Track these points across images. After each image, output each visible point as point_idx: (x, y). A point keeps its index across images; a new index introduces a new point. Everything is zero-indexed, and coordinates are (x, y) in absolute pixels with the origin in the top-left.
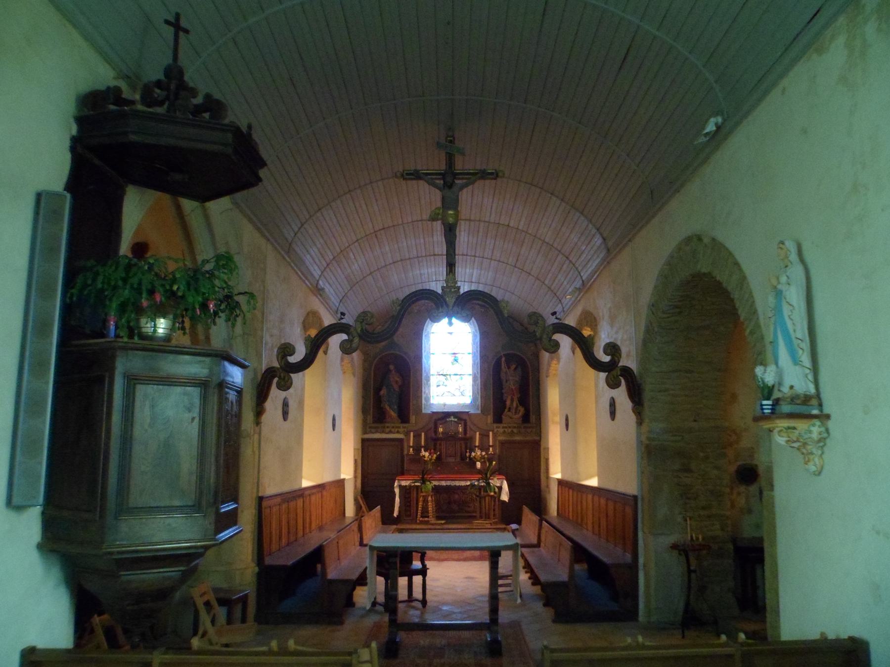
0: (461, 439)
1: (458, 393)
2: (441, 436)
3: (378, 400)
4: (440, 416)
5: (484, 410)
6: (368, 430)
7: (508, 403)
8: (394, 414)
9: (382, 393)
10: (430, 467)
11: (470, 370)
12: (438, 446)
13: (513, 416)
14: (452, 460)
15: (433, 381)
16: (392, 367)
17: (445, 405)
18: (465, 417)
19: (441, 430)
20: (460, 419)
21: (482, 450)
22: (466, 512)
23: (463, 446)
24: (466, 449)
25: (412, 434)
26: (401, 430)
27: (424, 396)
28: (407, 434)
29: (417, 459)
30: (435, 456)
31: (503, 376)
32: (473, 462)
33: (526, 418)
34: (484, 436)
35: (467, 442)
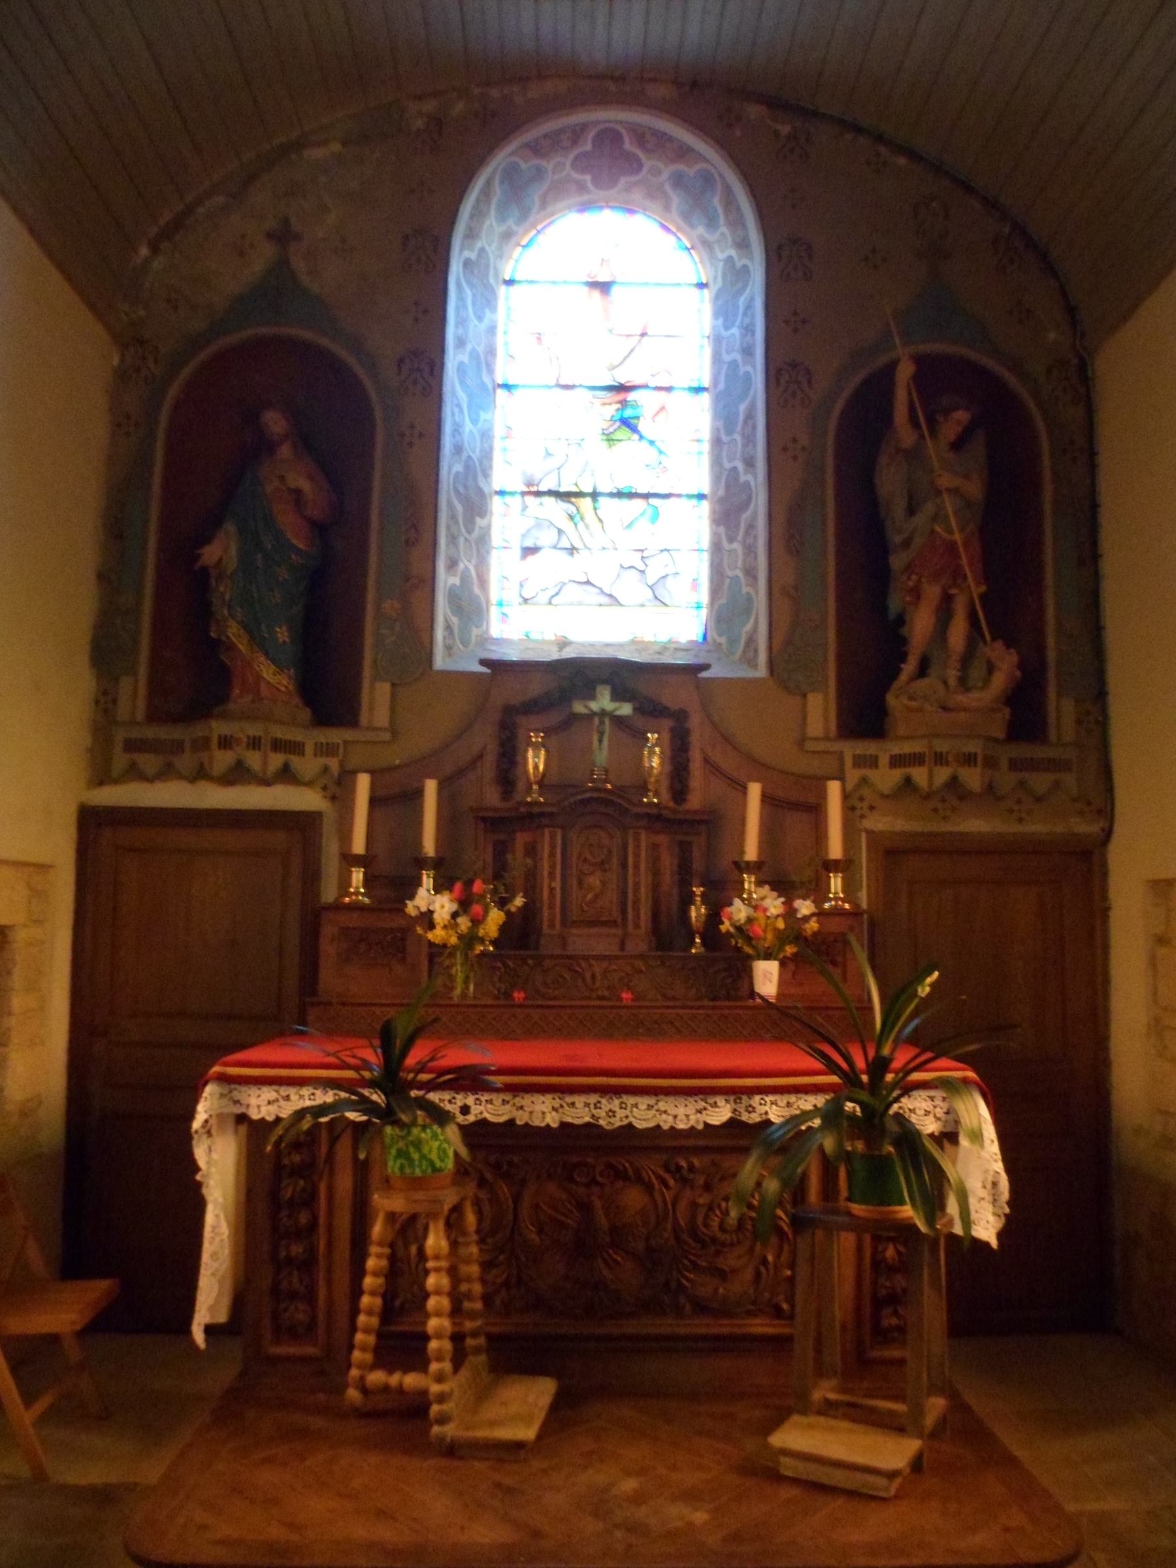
0: (656, 819)
1: (631, 589)
2: (535, 796)
3: (188, 598)
4: (536, 687)
5: (787, 662)
6: (120, 760)
7: (921, 624)
8: (274, 677)
9: (210, 554)
10: (461, 982)
11: (693, 470)
12: (517, 859)
13: (950, 697)
14: (600, 943)
15: (506, 522)
16: (275, 422)
17: (563, 644)
18: (673, 696)
19: (535, 761)
20: (651, 710)
21: (784, 886)
22: (701, 1308)
23: (668, 863)
24: (684, 884)
25: (363, 783)
26: (308, 765)
27: (445, 580)
28: (339, 789)
29: (387, 934)
30: (495, 918)
31: (890, 480)
32: (730, 958)
33: (1025, 714)
34: (795, 804)
35: (689, 833)
